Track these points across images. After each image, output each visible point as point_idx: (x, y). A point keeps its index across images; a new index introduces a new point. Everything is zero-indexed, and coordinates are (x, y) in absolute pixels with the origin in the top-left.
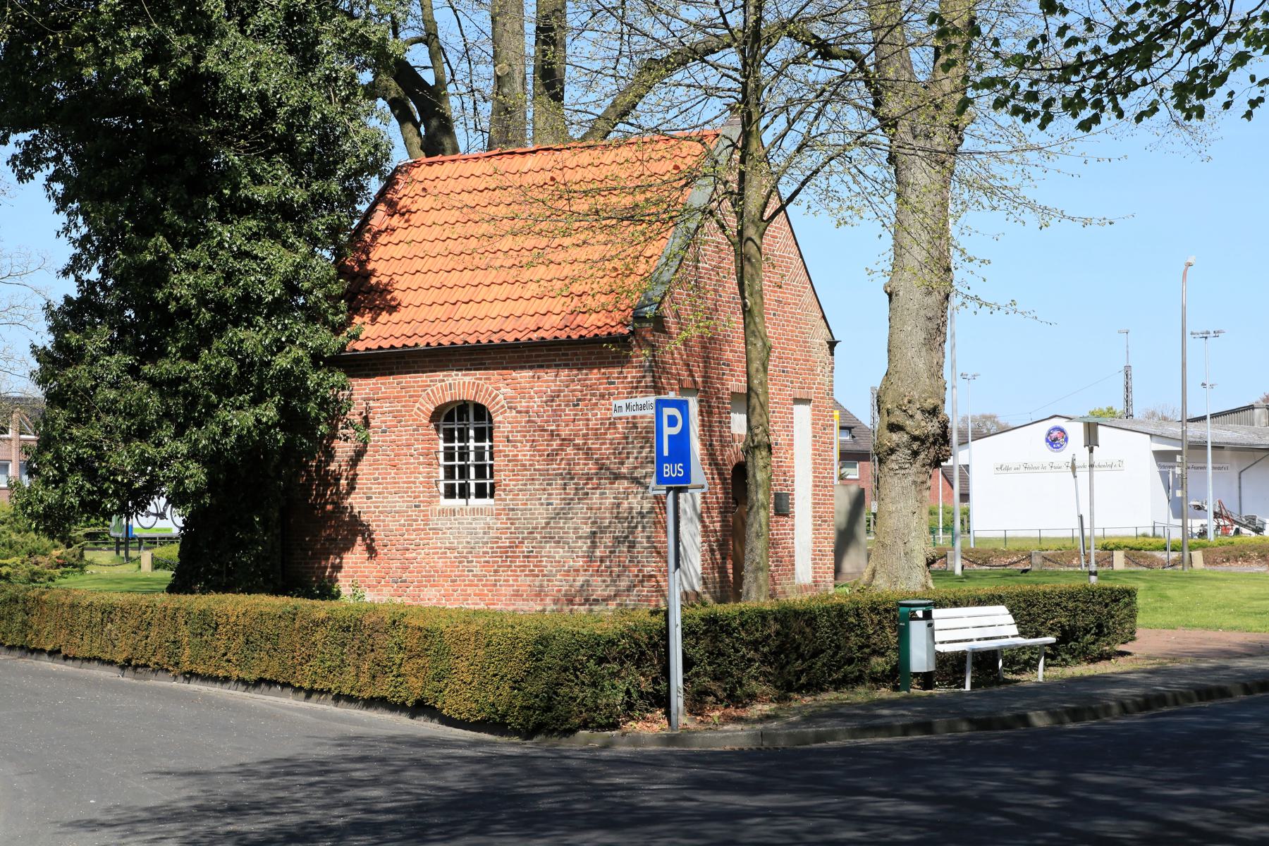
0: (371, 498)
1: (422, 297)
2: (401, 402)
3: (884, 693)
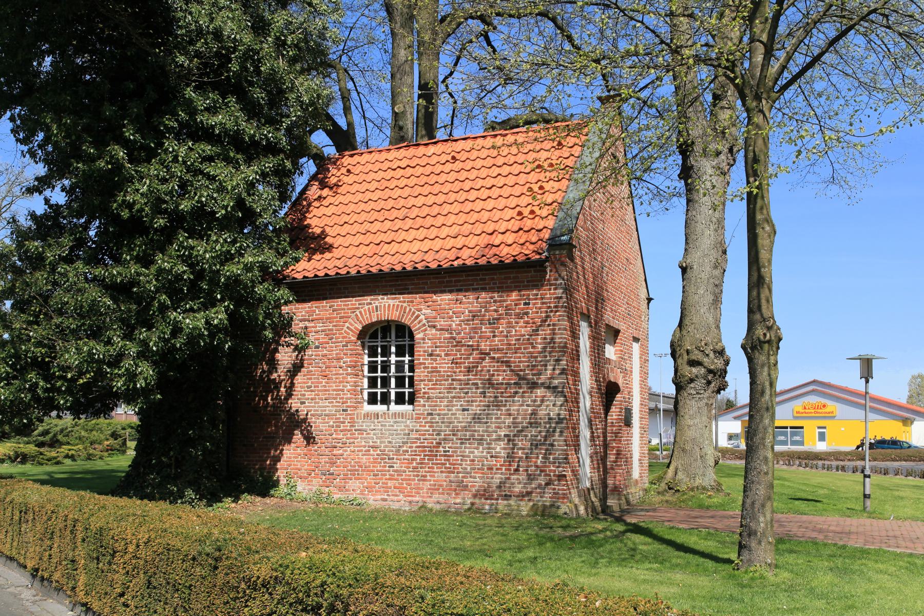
0: (304, 403)
1: (349, 240)
2: (333, 322)
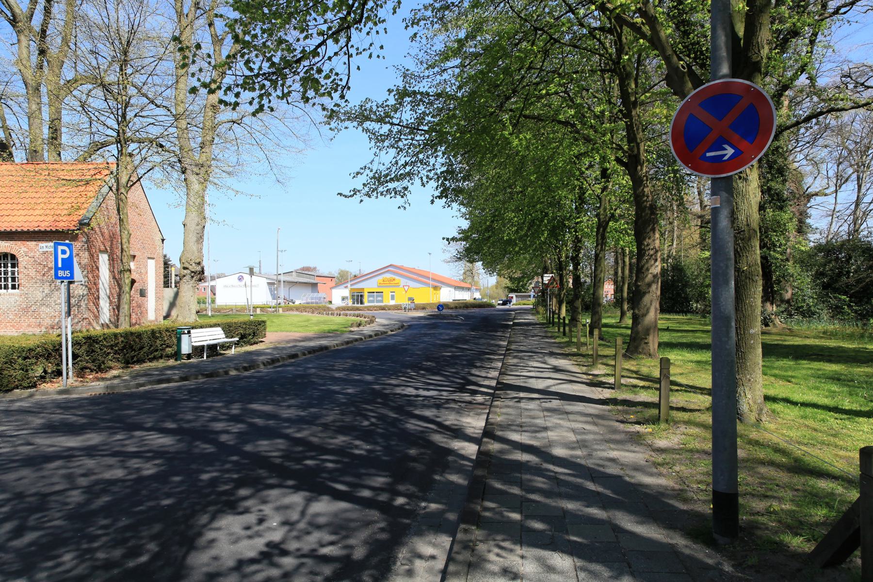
3: (171, 362)
